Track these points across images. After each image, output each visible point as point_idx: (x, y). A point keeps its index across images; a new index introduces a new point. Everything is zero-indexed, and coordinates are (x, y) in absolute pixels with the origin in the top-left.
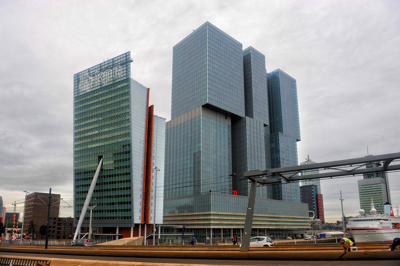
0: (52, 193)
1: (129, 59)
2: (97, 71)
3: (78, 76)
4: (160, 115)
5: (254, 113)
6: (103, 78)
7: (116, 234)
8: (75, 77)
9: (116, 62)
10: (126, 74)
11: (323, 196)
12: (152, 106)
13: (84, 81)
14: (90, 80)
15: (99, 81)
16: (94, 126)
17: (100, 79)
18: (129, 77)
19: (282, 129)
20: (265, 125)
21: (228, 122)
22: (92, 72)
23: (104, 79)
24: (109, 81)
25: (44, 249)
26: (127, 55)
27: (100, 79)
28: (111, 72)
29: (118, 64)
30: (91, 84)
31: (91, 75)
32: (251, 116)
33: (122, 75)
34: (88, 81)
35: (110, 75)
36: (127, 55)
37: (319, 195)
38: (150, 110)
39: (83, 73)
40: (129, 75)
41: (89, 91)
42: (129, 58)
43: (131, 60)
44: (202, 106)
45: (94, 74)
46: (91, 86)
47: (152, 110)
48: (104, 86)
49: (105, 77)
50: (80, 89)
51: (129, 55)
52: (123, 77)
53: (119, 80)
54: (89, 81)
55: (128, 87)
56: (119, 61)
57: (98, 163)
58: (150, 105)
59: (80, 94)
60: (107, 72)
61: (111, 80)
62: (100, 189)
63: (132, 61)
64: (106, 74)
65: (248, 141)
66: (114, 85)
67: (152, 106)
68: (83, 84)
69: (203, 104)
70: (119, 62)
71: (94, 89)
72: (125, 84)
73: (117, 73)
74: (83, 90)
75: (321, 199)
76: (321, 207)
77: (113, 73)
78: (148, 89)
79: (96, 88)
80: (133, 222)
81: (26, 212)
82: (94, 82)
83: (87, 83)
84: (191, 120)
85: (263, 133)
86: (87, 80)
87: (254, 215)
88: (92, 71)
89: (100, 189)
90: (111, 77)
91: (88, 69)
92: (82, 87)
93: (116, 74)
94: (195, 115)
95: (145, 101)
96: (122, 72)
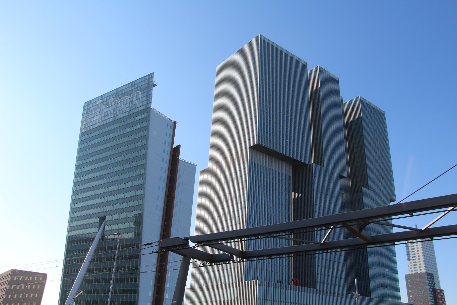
1: (152, 83)
2: (112, 99)
4: (188, 160)
5: (325, 158)
6: (118, 107)
8: (84, 107)
9: (136, 86)
11: (444, 292)
12: (179, 147)
14: (102, 110)
15: (112, 111)
18: (150, 106)
19: (363, 134)
20: (341, 177)
21: (287, 171)
22: (105, 99)
23: (119, 109)
24: (125, 112)
26: (150, 77)
27: (114, 109)
28: (129, 100)
29: (138, 89)
30: (103, 115)
31: (105, 103)
33: (142, 103)
34: (100, 111)
35: (126, 104)
36: (150, 77)
37: (438, 291)
38: (176, 151)
40: (150, 104)
42: (151, 81)
43: (155, 83)
44: (250, 147)
45: (108, 101)
47: (178, 152)
48: (118, 117)
49: (120, 106)
51: (153, 77)
52: (142, 106)
53: (137, 110)
54: (101, 111)
55: (147, 119)
56: (139, 85)
57: (98, 227)
58: (175, 146)
60: (124, 99)
61: (128, 110)
62: (94, 268)
63: (155, 85)
64: (122, 102)
65: (316, 201)
66: (129, 116)
67: (179, 147)
70: (139, 87)
71: (106, 122)
72: (143, 116)
73: (136, 100)
75: (441, 298)
76: (442, 300)
77: (130, 100)
78: (175, 123)
79: (108, 121)
81: (68, 259)
82: (107, 113)
85: (338, 189)
86: (98, 110)
88: (106, 98)
89: (94, 268)
90: (128, 105)
91: (102, 96)
93: (134, 103)
96: (141, 100)
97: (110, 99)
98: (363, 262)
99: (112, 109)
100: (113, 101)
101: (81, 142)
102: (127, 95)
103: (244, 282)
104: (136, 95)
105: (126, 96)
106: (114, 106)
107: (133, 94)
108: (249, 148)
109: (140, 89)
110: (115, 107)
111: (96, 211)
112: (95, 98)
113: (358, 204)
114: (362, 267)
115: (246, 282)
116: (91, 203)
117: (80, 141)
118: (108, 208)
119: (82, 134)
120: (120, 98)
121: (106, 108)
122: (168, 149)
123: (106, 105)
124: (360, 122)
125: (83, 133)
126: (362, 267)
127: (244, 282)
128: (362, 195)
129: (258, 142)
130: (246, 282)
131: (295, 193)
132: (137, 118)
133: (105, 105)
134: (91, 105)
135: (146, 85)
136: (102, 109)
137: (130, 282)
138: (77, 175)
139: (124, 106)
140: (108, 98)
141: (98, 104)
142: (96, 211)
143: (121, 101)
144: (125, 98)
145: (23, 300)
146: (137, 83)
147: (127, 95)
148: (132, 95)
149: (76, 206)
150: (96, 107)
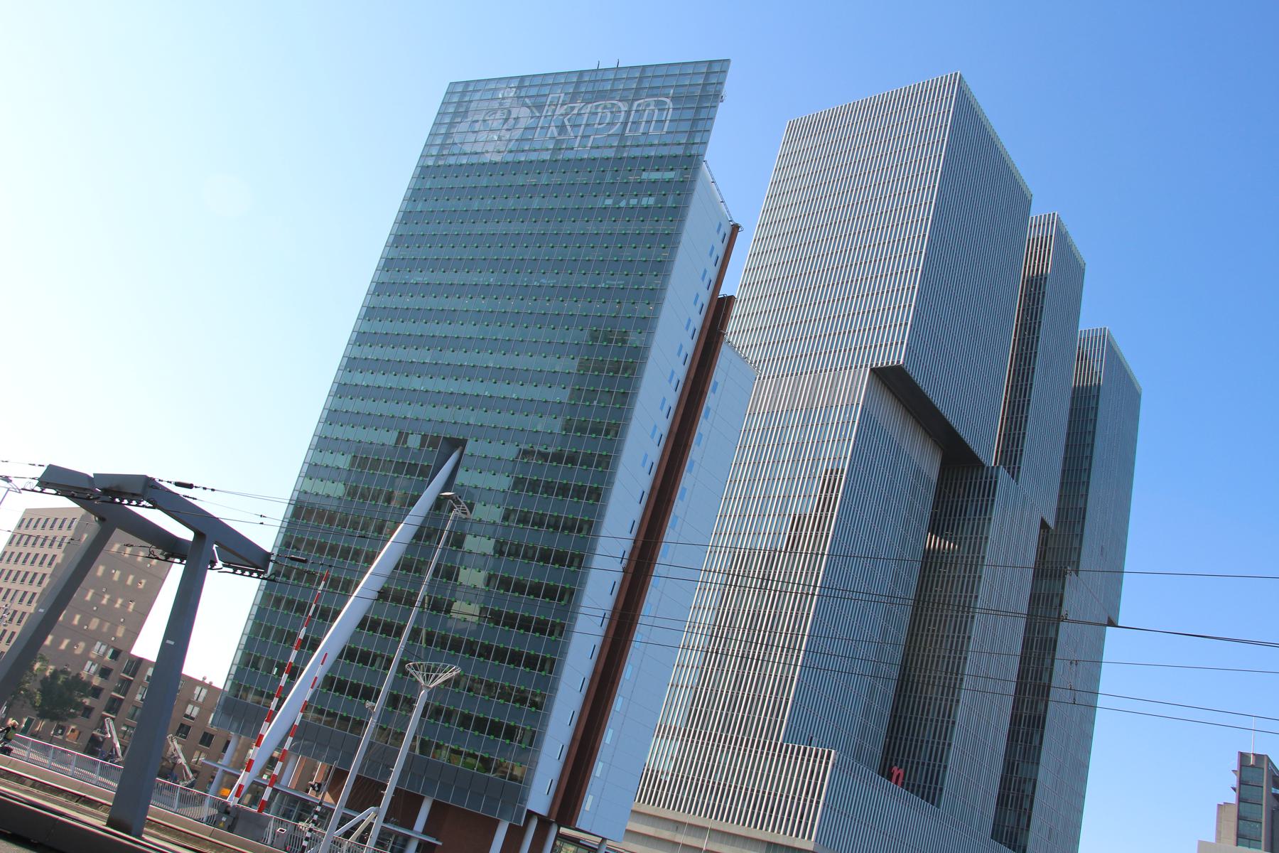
0: (653, 577)
3: (464, 93)
7: (411, 827)
8: (450, 93)
10: (688, 139)
13: (487, 118)
14: (517, 119)
15: (554, 131)
16: (466, 303)
17: (562, 128)
22: (533, 92)
25: (95, 821)
30: (517, 134)
32: (1014, 473)
35: (612, 124)
38: (720, 310)
39: (492, 86)
41: (497, 158)
44: (872, 370)
45: (543, 99)
46: (510, 140)
50: (456, 141)
59: (452, 161)
67: (730, 299)
68: (477, 127)
69: (880, 362)
72: (669, 175)
74: (467, 149)
78: (736, 228)
79: (533, 156)
80: (523, 800)
83: (496, 125)
84: (829, 407)
87: (203, 690)
91: (522, 78)
92: (471, 138)
94: (773, 400)
95: (712, 273)
97: (551, 96)
98: (1023, 762)
99: (553, 124)
100: (560, 102)
101: (415, 194)
102: (618, 99)
103: (782, 745)
104: (652, 107)
105: (615, 102)
106: (561, 117)
107: (642, 101)
108: (868, 369)
109: (671, 95)
110: (567, 123)
111: (518, 421)
112: (485, 80)
113: (1044, 607)
114: (1017, 773)
115: (788, 746)
116: (417, 383)
117: (414, 189)
118: (490, 418)
119: (424, 172)
120: (591, 103)
121: (532, 117)
122: (705, 298)
123: (534, 110)
124: (1094, 396)
125: (428, 167)
126: (1017, 773)
127: (782, 745)
128: (1063, 588)
129: (904, 363)
130: (788, 746)
131: (938, 538)
132: (645, 175)
133: (529, 107)
134: (477, 96)
135: (698, 92)
136: (514, 115)
137: (522, 668)
138: (379, 288)
139: (600, 126)
140: (546, 91)
141: (503, 98)
142: (518, 421)
143: (593, 110)
144: (609, 106)
145: (95, 608)
146: (478, 98)
147: (620, 101)
148: (639, 105)
149: (359, 378)
150: (495, 105)
